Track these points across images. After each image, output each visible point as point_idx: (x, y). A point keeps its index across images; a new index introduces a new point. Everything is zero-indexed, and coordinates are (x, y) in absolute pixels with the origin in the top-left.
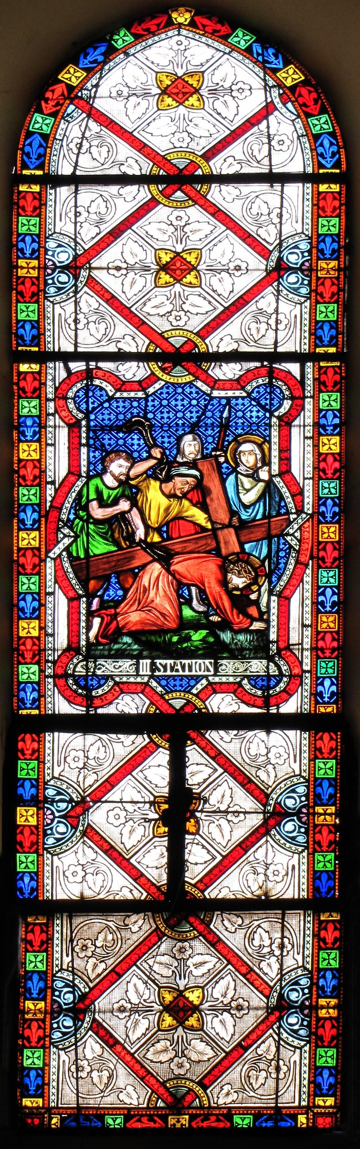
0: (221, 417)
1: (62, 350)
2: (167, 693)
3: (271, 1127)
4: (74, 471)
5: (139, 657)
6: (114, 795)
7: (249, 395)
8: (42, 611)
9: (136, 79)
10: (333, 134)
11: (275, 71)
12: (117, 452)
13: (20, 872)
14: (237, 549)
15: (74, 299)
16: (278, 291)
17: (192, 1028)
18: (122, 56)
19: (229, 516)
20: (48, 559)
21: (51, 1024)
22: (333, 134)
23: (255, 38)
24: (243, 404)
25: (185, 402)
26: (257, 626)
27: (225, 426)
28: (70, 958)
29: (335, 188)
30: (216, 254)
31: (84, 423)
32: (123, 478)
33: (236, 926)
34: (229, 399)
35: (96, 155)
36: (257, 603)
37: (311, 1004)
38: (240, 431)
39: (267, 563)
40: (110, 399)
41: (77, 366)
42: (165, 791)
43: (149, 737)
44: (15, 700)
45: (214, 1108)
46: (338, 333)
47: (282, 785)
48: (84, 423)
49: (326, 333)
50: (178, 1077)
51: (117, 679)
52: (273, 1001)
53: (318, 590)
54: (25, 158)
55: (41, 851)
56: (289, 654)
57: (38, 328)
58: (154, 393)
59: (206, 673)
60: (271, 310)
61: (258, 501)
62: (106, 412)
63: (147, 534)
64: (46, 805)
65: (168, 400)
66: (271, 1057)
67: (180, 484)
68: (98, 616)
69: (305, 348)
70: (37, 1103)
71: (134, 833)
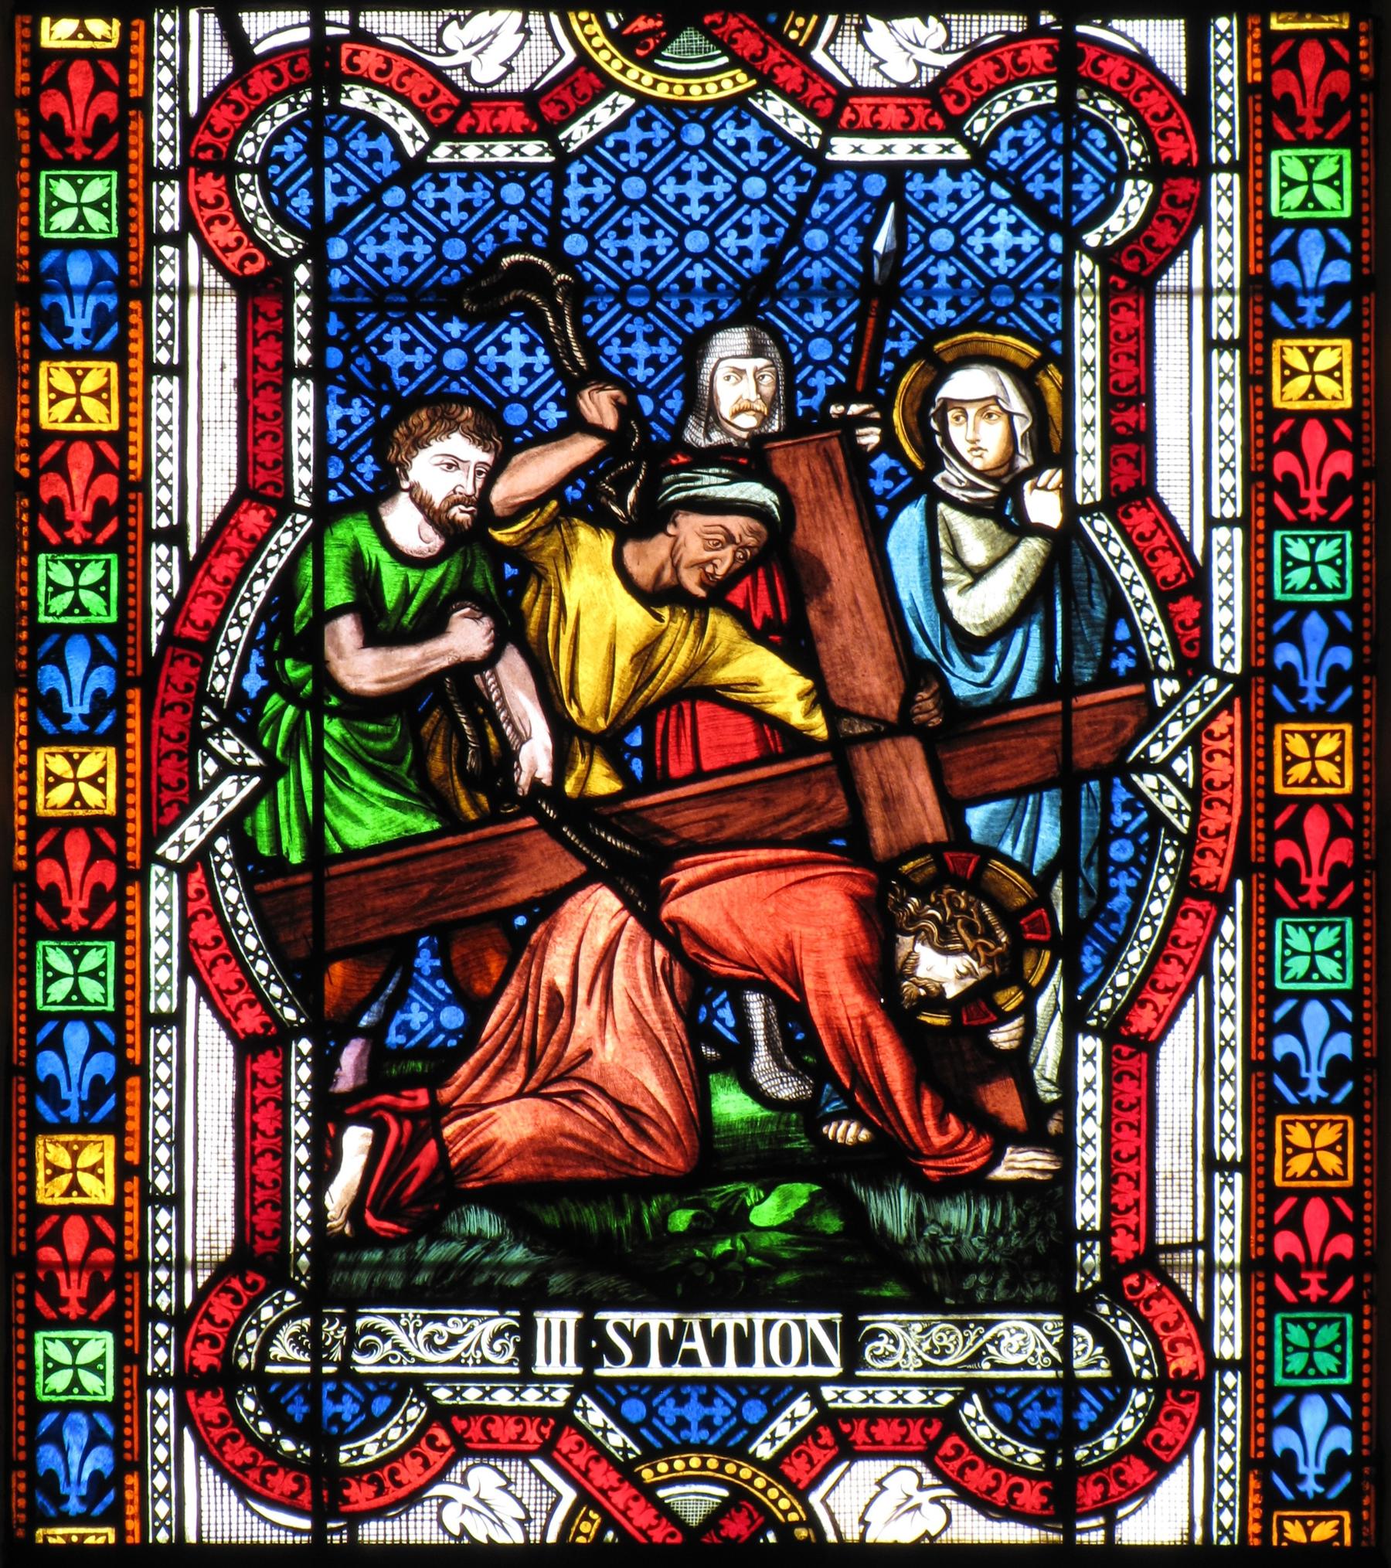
2: (650, 1455)
7: (980, 154)
8: (133, 1096)
19: (899, 683)
20: (157, 870)
24: (956, 197)
34: (896, 172)
36: (1019, 1062)
38: (942, 314)
59: (811, 1370)
62: (394, 227)
63: (562, 763)
65: (648, 178)
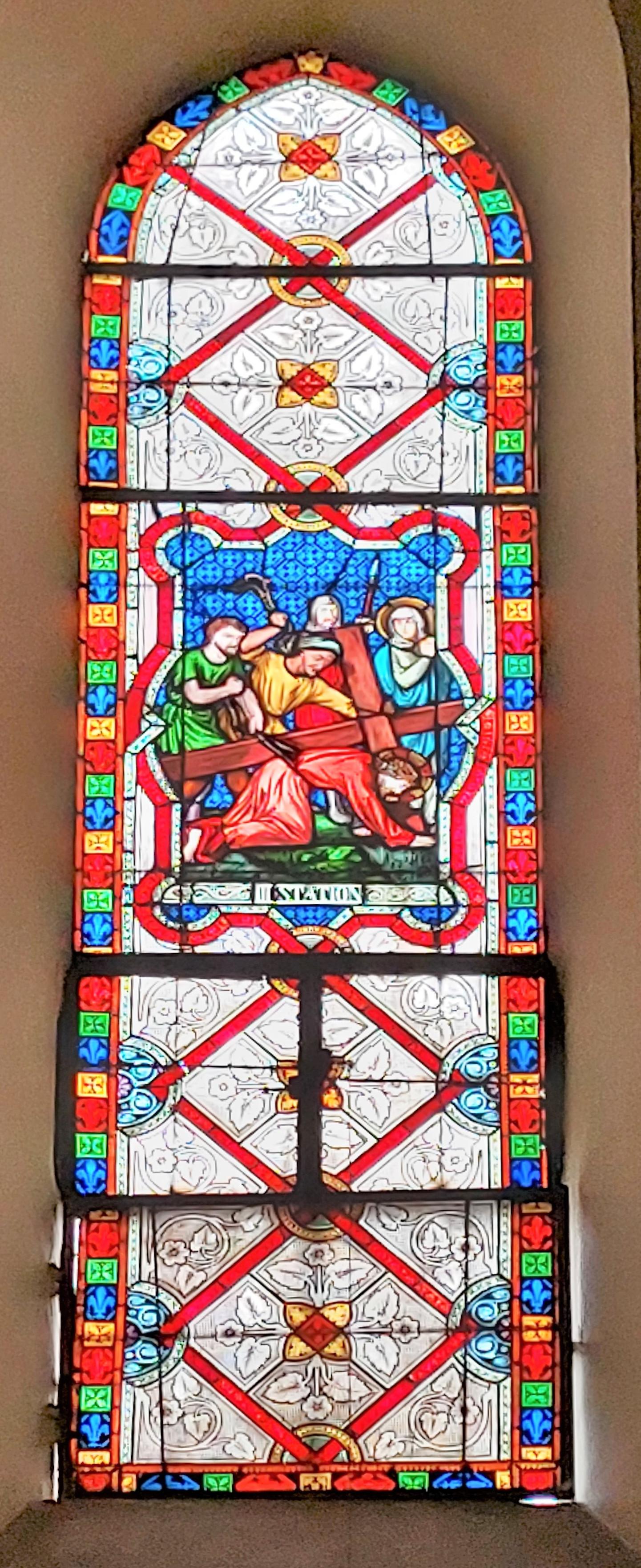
0: (368, 576)
1: (149, 487)
3: (457, 1489)
4: (164, 642)
5: (255, 879)
6: (219, 1056)
7: (406, 546)
8: (119, 821)
9: (250, 140)
10: (513, 215)
11: (434, 134)
12: (224, 618)
13: (80, 1159)
14: (393, 744)
15: (166, 422)
16: (444, 415)
17: (334, 1357)
18: (232, 111)
19: (380, 700)
20: (127, 755)
21: (124, 1354)
22: (513, 215)
23: (407, 91)
24: (398, 559)
25: (319, 555)
26: (421, 841)
27: (373, 587)
28: (152, 1267)
29: (518, 283)
30: (359, 365)
31: (178, 580)
32: (233, 651)
33: (398, 1222)
34: (378, 553)
35: (197, 239)
36: (421, 811)
37: (511, 1324)
38: (392, 593)
39: (434, 761)
40: (214, 551)
41: (169, 509)
42: (294, 1053)
43: (269, 983)
44: (78, 934)
45: (370, 1463)
46: (525, 469)
47: (461, 1046)
48: (178, 580)
49: (509, 469)
50: (315, 1423)
51: (224, 909)
52: (455, 1320)
53: (505, 795)
54: (102, 240)
55: (112, 1131)
56: (467, 877)
57: (117, 459)
58: (275, 544)
59: (351, 902)
60: (434, 438)
61: (421, 680)
62: (210, 566)
63: (265, 724)
64: (121, 1072)
66: (456, 1395)
67: (312, 660)
68: (198, 827)
69: (482, 488)
70: (101, 1457)
71: (248, 1108)
